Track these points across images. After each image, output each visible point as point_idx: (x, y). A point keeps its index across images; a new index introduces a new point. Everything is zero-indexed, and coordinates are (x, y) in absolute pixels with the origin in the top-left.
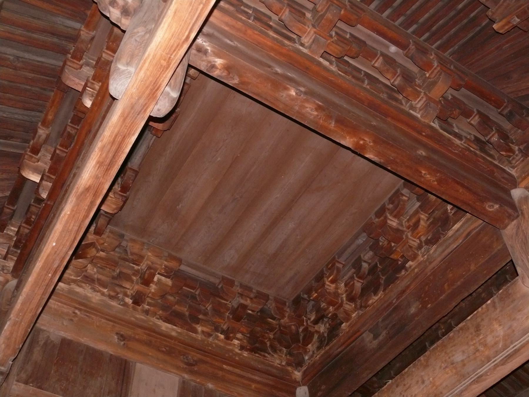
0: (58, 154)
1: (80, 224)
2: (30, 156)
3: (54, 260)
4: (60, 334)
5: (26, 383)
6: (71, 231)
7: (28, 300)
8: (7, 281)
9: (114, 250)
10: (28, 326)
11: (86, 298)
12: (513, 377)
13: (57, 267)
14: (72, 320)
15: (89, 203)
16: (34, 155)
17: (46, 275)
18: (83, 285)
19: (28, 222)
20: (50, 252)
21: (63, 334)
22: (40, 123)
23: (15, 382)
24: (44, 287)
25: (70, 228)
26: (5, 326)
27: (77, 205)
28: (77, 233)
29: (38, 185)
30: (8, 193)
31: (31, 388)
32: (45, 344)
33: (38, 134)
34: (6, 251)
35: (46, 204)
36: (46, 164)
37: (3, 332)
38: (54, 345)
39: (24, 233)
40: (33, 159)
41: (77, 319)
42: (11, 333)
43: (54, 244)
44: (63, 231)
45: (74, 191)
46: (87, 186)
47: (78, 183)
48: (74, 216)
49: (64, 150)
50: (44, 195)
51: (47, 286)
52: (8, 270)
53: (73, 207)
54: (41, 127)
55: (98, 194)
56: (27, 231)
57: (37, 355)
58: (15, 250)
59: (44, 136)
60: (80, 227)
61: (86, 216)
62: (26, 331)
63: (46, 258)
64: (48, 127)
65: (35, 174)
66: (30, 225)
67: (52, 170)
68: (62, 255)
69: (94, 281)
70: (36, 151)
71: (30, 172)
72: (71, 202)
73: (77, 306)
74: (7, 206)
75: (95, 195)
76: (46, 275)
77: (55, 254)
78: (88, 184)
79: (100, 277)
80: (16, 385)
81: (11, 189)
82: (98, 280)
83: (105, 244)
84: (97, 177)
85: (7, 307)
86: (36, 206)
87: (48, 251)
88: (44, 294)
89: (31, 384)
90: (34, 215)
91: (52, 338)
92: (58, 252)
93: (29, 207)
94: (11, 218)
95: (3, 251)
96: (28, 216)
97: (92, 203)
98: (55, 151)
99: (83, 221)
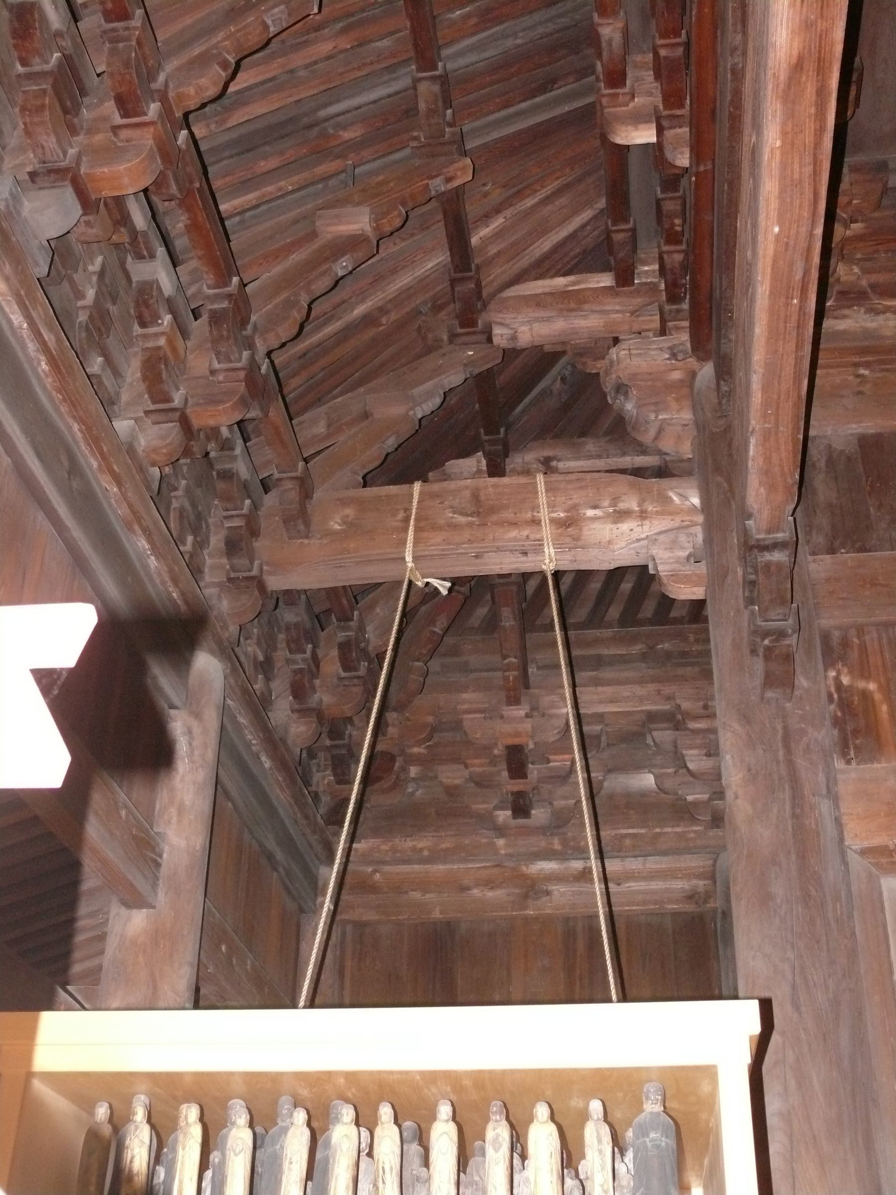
0: (665, 58)
1: (815, 155)
2: (610, 95)
3: (791, 264)
4: (849, 432)
5: (832, 550)
6: (801, 181)
7: (772, 373)
8: (693, 375)
9: (878, 207)
10: (796, 428)
11: (867, 334)
12: (577, 997)
13: (804, 277)
14: (860, 393)
15: (814, 97)
16: (618, 91)
17: (787, 304)
18: (846, 312)
19: (672, 238)
20: (775, 250)
21: (855, 428)
22: (596, 15)
23: (810, 558)
24: (794, 333)
25: (796, 176)
26: (747, 450)
27: (790, 115)
28: (815, 180)
29: (659, 146)
30: (602, 203)
31: (847, 557)
32: (831, 462)
33: (603, 40)
34: (658, 317)
35: (697, 174)
36: (650, 94)
37: (750, 463)
38: (849, 459)
39: (677, 265)
40: (621, 98)
41: (868, 386)
42: (768, 459)
43: (777, 229)
44: (782, 191)
45: (770, 87)
46: (794, 61)
47: (770, 63)
48: (793, 144)
49: (673, 41)
50: (683, 159)
51: (798, 327)
52: (685, 352)
53: (784, 124)
54: (600, 21)
55: (827, 64)
56: (678, 257)
57: (823, 489)
58: (675, 307)
59: (617, 38)
60: (816, 162)
61: (821, 130)
62: (795, 441)
63: (773, 269)
64: (615, 13)
65: (641, 126)
66: (679, 242)
67: (672, 98)
68: (803, 244)
69: (865, 293)
70: (616, 78)
71: (630, 128)
72: (774, 116)
73: (857, 359)
74: (614, 228)
75: (821, 70)
76: (787, 304)
77: (786, 250)
78: (795, 53)
79: (874, 278)
80: (814, 561)
81: (604, 191)
82: (873, 286)
83: (855, 202)
84: (807, 26)
85: (721, 422)
86: (671, 198)
87: (771, 252)
88: (799, 347)
89: (843, 551)
90: (677, 217)
91: (838, 445)
92: (792, 243)
93: (658, 202)
94: (634, 249)
95: (652, 321)
96: (666, 226)
97: (821, 92)
98: (656, 54)
99: (817, 144)
